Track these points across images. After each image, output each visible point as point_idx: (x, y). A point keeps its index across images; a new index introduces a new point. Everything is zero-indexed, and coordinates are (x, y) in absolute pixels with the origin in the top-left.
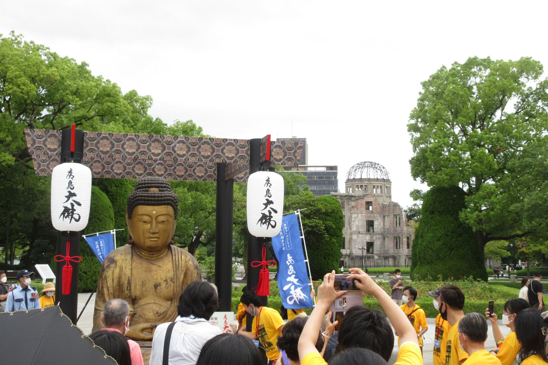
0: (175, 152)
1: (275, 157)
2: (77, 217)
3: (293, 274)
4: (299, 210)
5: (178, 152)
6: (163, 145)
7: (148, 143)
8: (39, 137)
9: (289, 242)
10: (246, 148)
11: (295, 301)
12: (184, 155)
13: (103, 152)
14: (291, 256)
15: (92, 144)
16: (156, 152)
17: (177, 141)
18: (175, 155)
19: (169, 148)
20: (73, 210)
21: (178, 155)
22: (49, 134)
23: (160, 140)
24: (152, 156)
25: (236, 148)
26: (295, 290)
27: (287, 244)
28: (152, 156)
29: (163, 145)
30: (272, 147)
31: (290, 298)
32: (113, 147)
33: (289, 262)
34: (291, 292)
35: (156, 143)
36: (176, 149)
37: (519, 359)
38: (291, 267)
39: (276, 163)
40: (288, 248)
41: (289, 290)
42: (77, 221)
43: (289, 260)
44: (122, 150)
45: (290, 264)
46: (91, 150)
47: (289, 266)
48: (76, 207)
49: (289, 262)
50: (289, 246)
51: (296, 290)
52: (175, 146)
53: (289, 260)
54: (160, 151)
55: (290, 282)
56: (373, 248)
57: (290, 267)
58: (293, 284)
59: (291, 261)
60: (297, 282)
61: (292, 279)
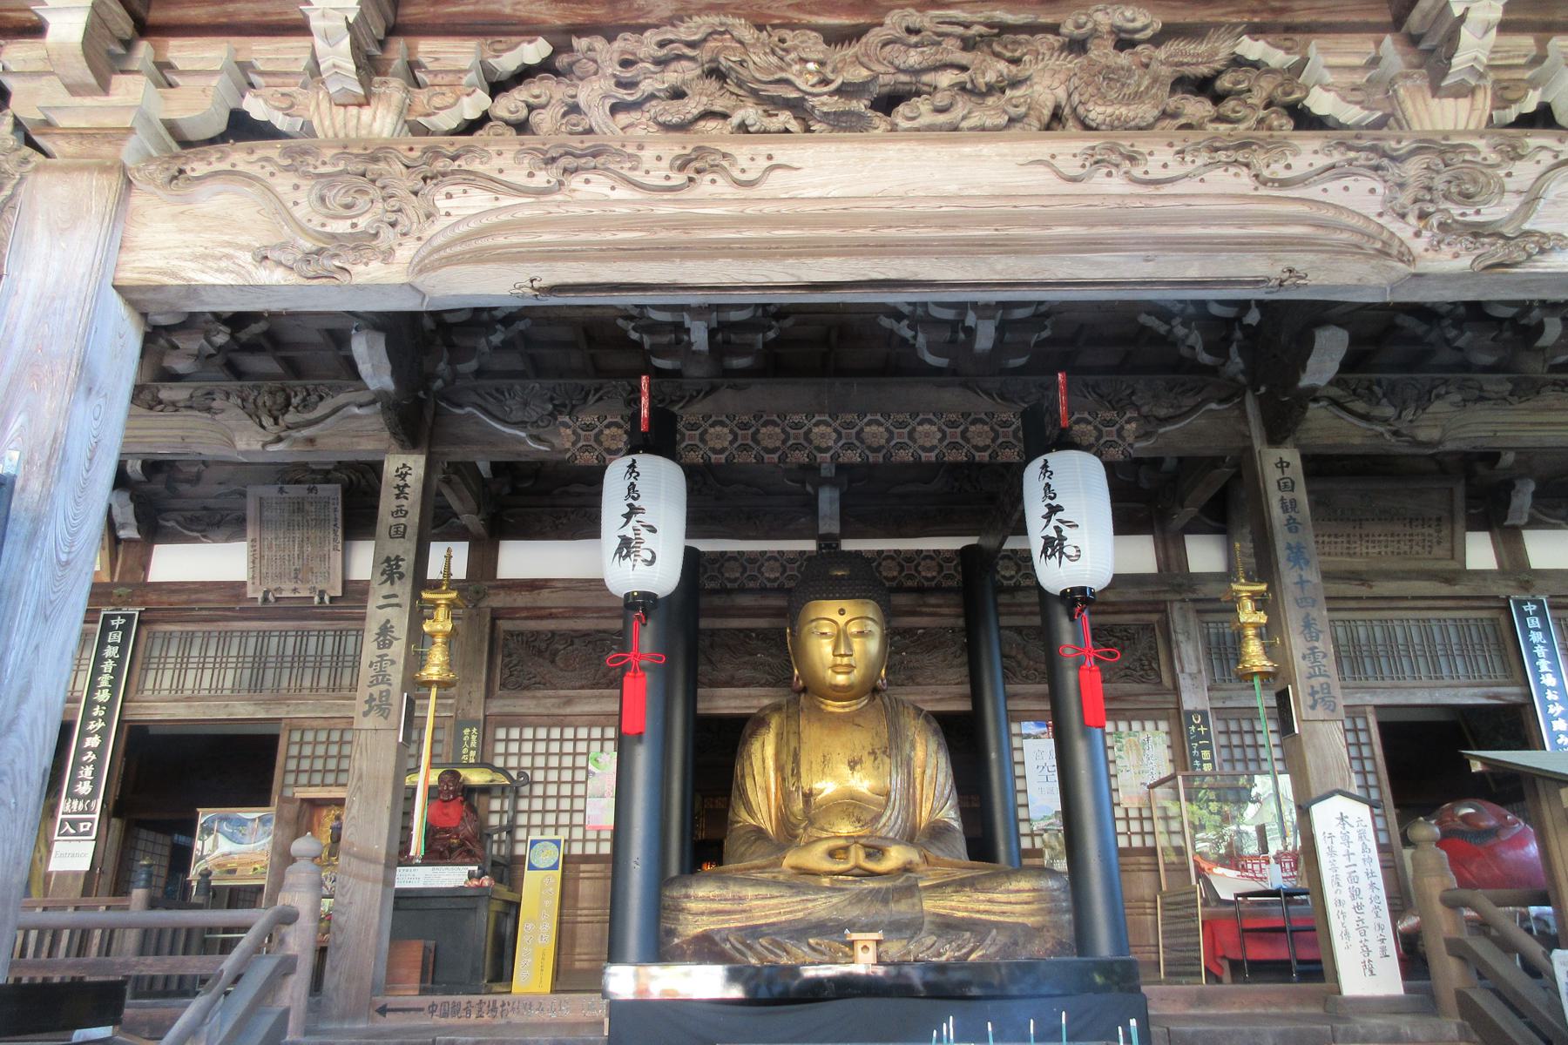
0: (835, 430)
1: (620, 431)
5: (829, 430)
6: (862, 442)
7: (1102, 441)
8: (902, 446)
10: (683, 445)
12: (608, 426)
13: (775, 424)
15: (587, 439)
16: (874, 428)
17: (832, 452)
18: (836, 424)
19: (848, 436)
21: (828, 425)
22: (884, 451)
23: (867, 452)
24: (1090, 418)
25: (915, 442)
28: (1090, 418)
29: (862, 442)
32: (963, 434)
35: (875, 445)
36: (834, 435)
37: (963, 10)
39: (618, 419)
44: (736, 429)
46: (1005, 424)
52: (836, 442)
54: (867, 429)
56: (1489, 302)
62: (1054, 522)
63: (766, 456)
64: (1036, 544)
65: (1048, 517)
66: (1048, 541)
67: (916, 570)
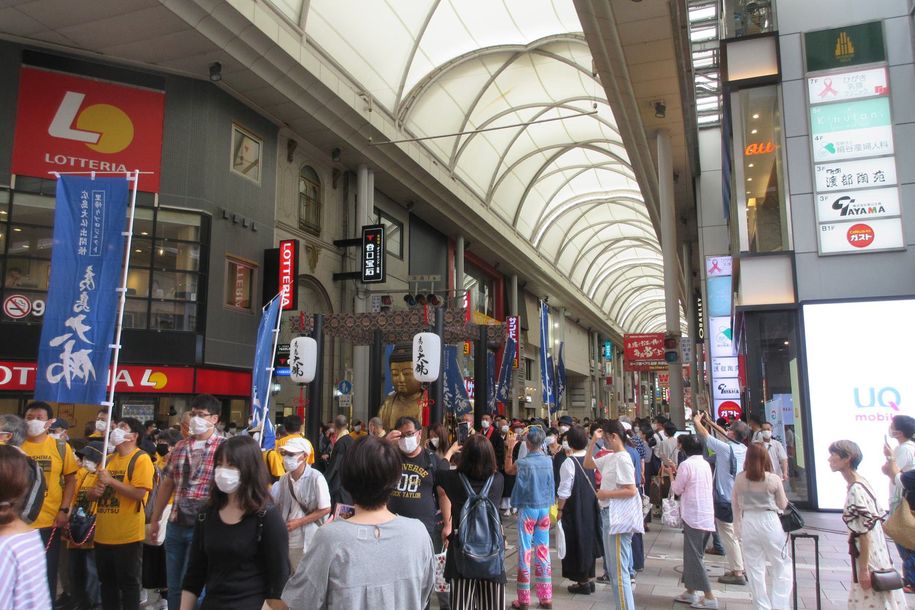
2: (301, 373)
3: (82, 312)
4: (137, 171)
9: (99, 240)
11: (63, 379)
14: (93, 271)
18: (378, 325)
20: (298, 368)
21: (380, 325)
26: (73, 352)
27: (93, 243)
30: (488, 329)
31: (56, 367)
33: (85, 284)
34: (61, 356)
38: (84, 297)
40: (93, 252)
41: (61, 349)
42: (301, 375)
43: (87, 281)
45: (86, 290)
47: (81, 293)
48: (299, 366)
49: (85, 284)
50: (96, 249)
51: (76, 355)
53: (87, 281)
55: (70, 330)
57: (82, 296)
58: (75, 336)
59: (88, 283)
60: (85, 333)
61: (77, 324)
62: (421, 360)
63: (417, 312)
64: (414, 366)
65: (419, 358)
66: (418, 366)
67: (410, 320)
